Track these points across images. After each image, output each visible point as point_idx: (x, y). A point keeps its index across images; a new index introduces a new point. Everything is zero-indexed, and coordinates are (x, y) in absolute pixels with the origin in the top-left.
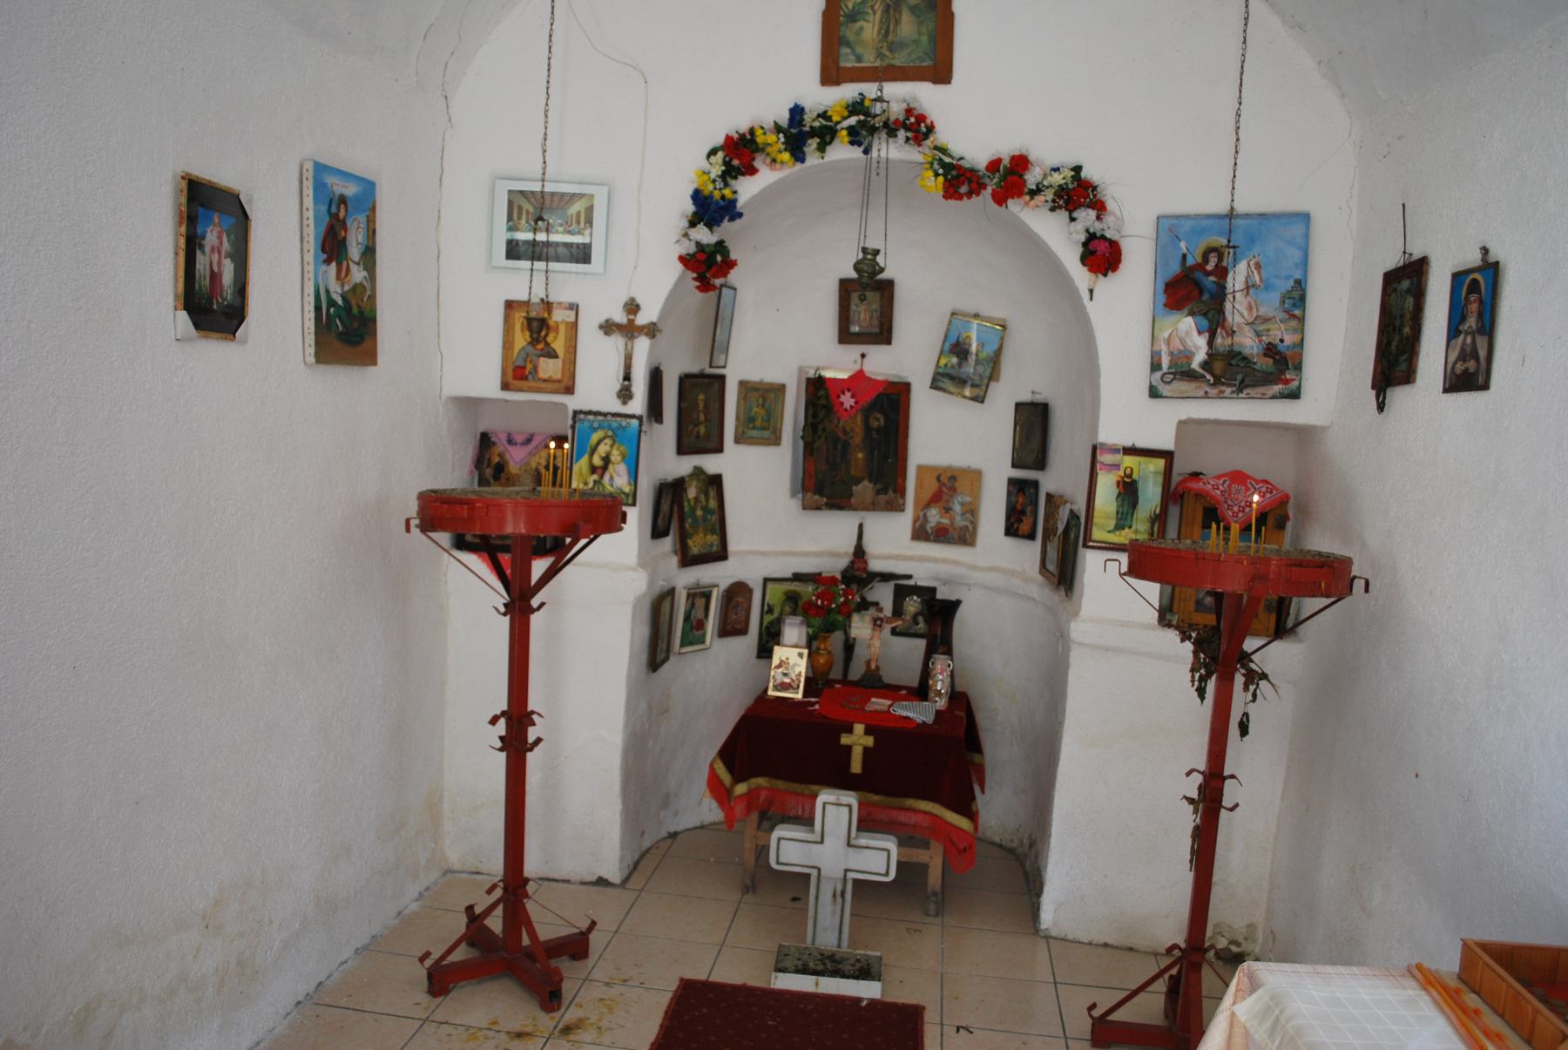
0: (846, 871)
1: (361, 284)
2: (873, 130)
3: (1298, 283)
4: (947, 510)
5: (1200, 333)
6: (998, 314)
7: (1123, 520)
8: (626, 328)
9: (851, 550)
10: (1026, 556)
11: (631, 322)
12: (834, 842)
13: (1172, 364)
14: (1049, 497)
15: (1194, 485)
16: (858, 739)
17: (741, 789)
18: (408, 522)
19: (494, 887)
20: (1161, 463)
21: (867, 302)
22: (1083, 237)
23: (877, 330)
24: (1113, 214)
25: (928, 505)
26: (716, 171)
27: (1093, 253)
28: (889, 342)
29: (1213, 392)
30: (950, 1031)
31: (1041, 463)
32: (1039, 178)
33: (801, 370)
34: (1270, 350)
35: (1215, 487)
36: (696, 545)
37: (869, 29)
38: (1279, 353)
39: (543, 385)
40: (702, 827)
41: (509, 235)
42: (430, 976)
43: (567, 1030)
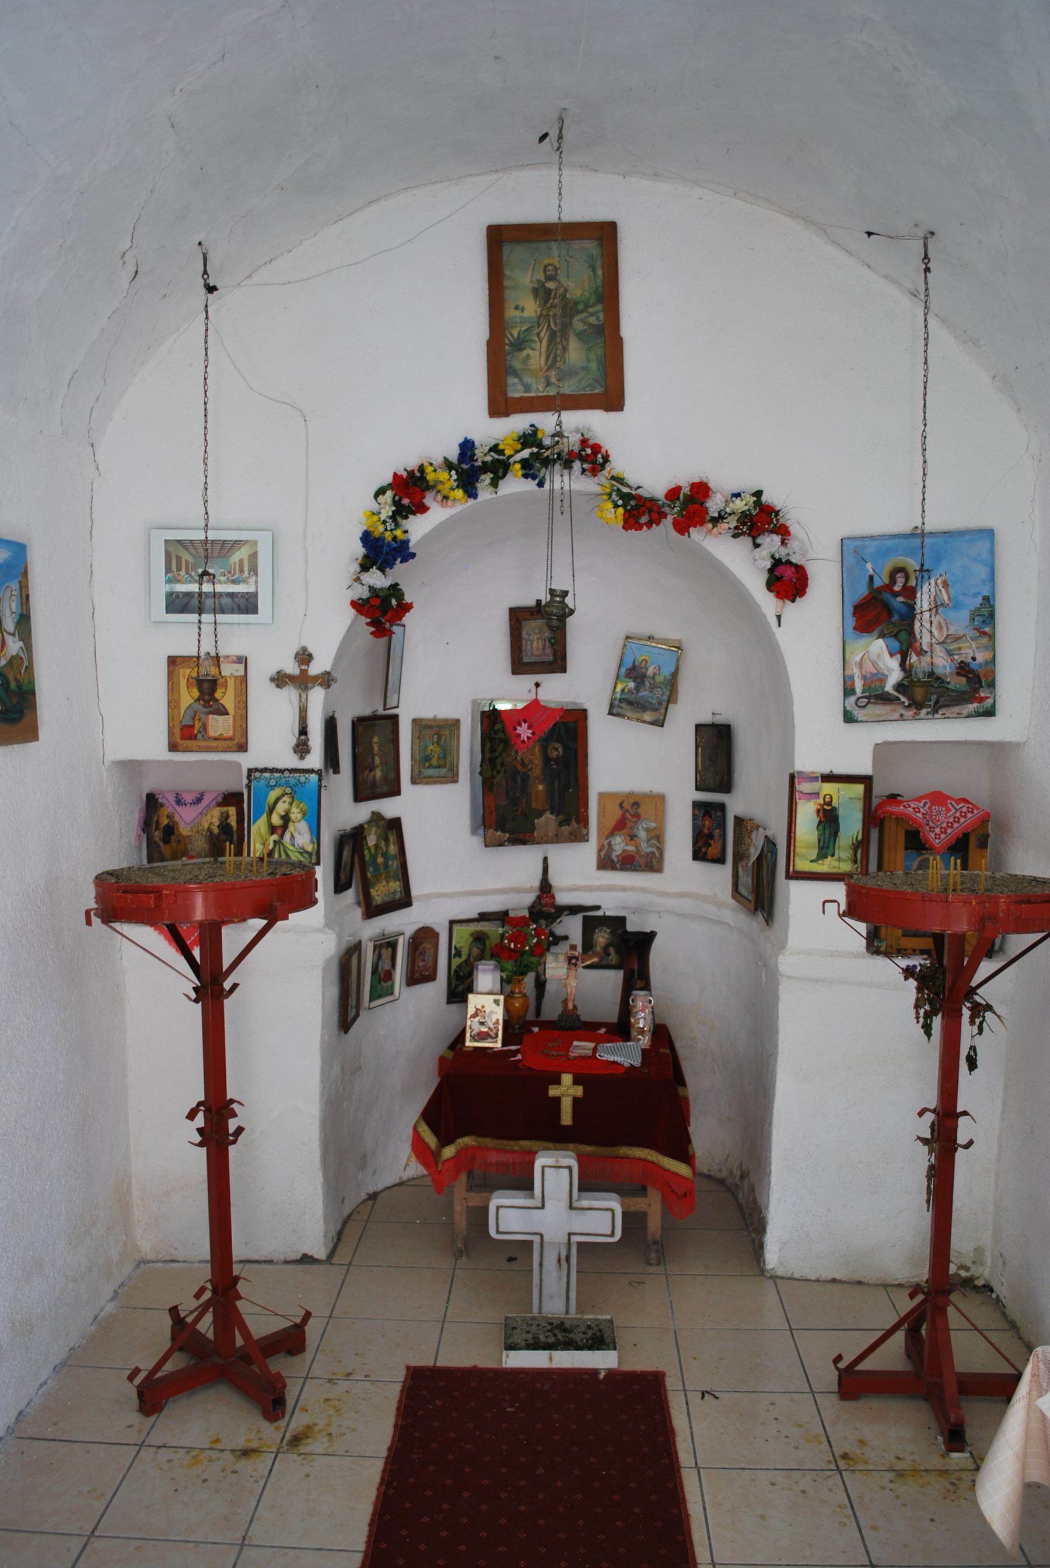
0: (570, 1234)
1: (17, 655)
2: (547, 462)
3: (986, 599)
4: (632, 837)
5: (891, 655)
6: (673, 635)
7: (825, 849)
8: (298, 679)
9: (537, 884)
10: (717, 879)
11: (304, 672)
12: (554, 1206)
13: (866, 688)
14: (739, 821)
15: (894, 809)
16: (566, 1090)
17: (449, 1152)
18: (88, 913)
19: (203, 1289)
20: (859, 789)
21: (539, 634)
22: (768, 564)
23: (551, 658)
24: (796, 538)
25: (612, 833)
26: (387, 511)
27: (779, 579)
28: (563, 670)
29: (909, 713)
30: (695, 1398)
31: (726, 785)
32: (721, 506)
33: (475, 703)
34: (963, 669)
35: (916, 810)
36: (379, 893)
37: (536, 356)
38: (971, 671)
39: (214, 744)
40: (401, 1184)
41: (168, 588)
42: (141, 1394)
43: (296, 1441)
